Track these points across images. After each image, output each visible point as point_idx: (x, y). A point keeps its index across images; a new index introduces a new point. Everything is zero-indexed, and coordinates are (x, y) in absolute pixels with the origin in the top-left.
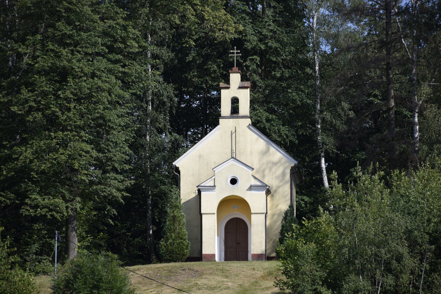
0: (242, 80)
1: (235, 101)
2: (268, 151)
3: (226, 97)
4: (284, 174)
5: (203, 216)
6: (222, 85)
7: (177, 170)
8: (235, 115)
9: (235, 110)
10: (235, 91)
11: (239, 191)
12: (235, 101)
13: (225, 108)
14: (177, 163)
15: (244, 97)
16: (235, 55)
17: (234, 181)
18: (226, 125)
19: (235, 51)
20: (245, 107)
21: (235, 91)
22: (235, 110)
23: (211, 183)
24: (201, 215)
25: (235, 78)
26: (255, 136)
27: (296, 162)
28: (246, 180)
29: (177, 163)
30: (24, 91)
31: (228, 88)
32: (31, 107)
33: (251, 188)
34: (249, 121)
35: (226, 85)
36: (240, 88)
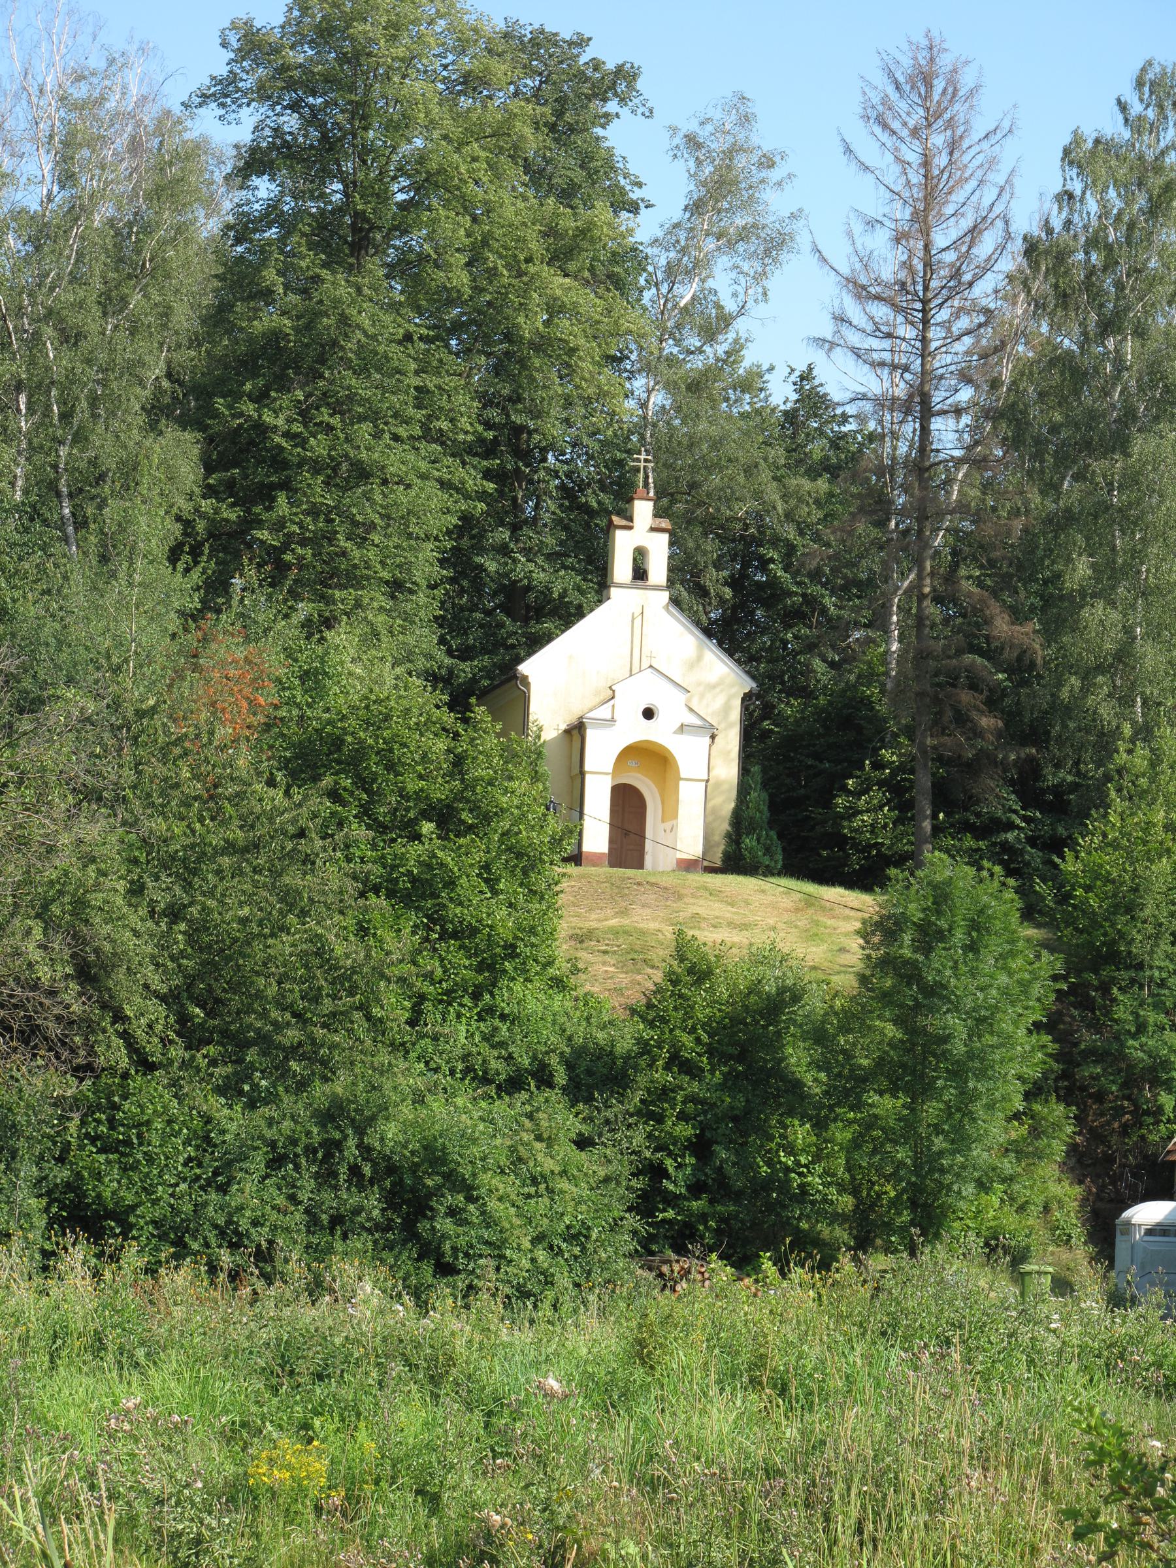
0: (656, 515)
1: (640, 555)
2: (700, 658)
3: (623, 545)
4: (726, 708)
5: (588, 777)
6: (616, 520)
7: (525, 680)
8: (640, 583)
9: (640, 574)
10: (641, 536)
11: (658, 733)
12: (640, 555)
13: (622, 569)
14: (524, 668)
15: (659, 550)
16: (642, 464)
17: (649, 714)
18: (623, 600)
19: (642, 457)
20: (658, 571)
21: (641, 536)
22: (640, 574)
23: (604, 712)
24: (582, 774)
25: (643, 510)
26: (681, 628)
27: (754, 685)
28: (672, 712)
29: (524, 668)
30: (282, 499)
31: (631, 528)
32: (290, 535)
33: (682, 729)
34: (665, 596)
35: (624, 523)
36: (652, 529)
